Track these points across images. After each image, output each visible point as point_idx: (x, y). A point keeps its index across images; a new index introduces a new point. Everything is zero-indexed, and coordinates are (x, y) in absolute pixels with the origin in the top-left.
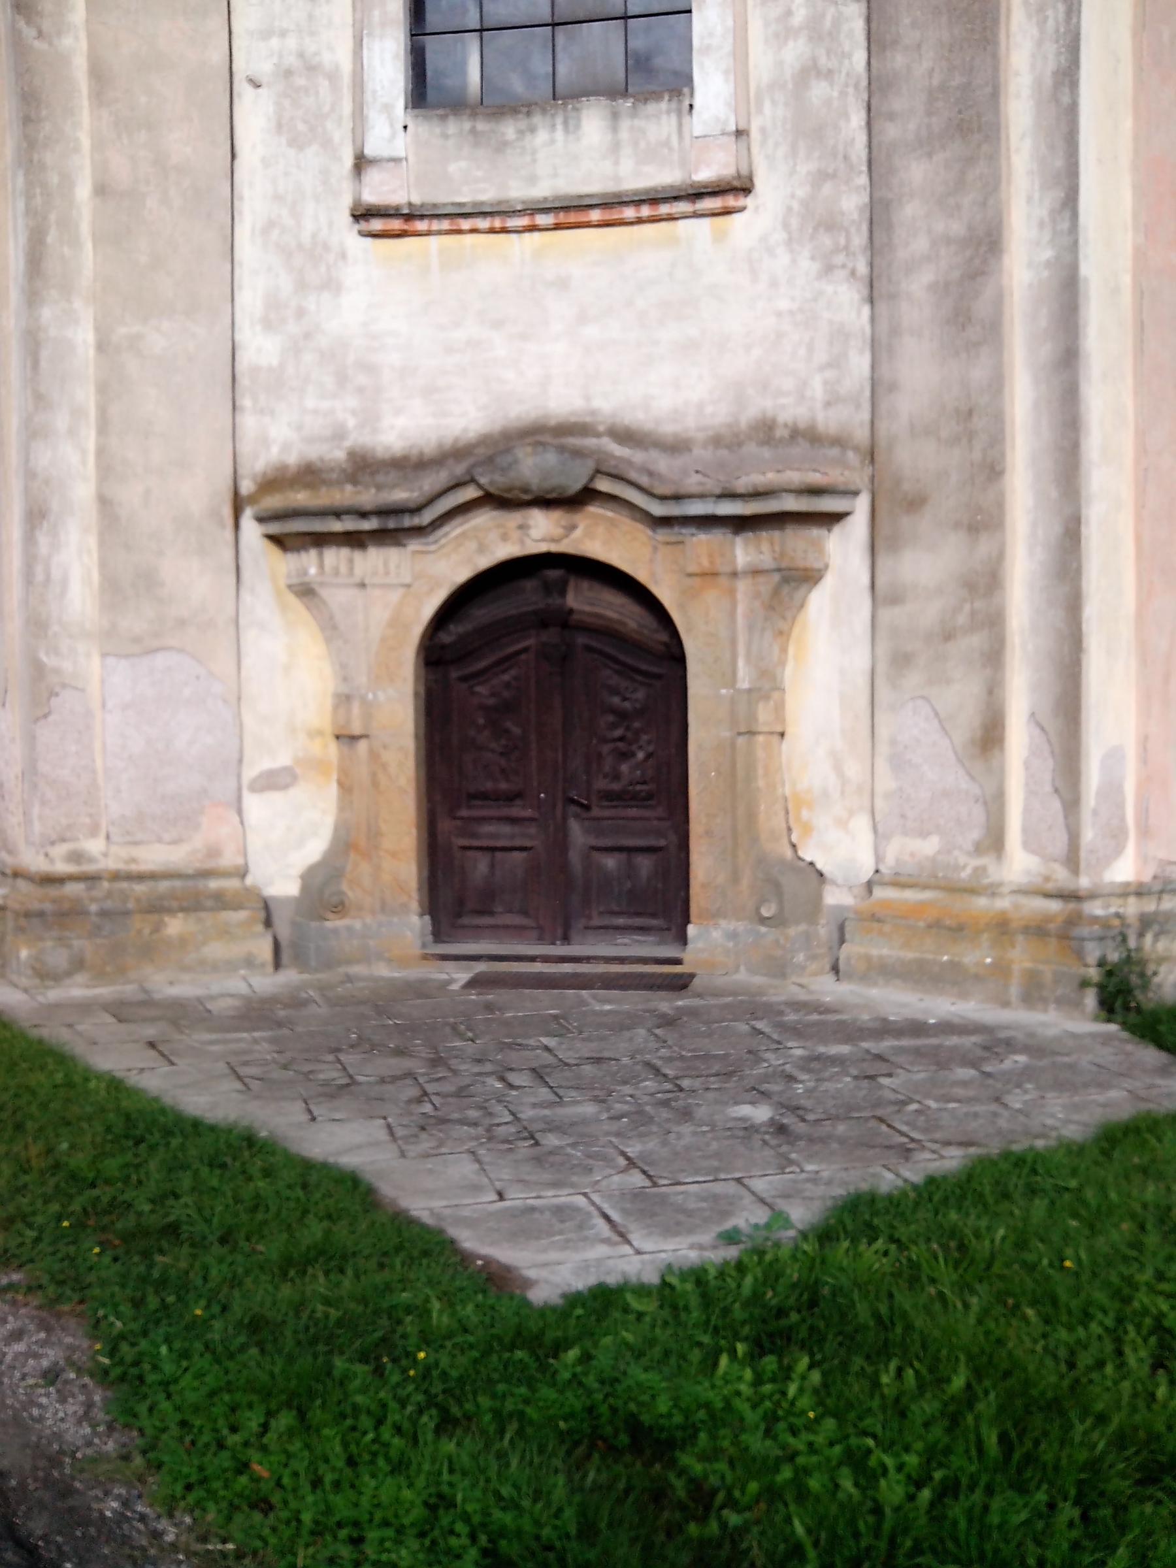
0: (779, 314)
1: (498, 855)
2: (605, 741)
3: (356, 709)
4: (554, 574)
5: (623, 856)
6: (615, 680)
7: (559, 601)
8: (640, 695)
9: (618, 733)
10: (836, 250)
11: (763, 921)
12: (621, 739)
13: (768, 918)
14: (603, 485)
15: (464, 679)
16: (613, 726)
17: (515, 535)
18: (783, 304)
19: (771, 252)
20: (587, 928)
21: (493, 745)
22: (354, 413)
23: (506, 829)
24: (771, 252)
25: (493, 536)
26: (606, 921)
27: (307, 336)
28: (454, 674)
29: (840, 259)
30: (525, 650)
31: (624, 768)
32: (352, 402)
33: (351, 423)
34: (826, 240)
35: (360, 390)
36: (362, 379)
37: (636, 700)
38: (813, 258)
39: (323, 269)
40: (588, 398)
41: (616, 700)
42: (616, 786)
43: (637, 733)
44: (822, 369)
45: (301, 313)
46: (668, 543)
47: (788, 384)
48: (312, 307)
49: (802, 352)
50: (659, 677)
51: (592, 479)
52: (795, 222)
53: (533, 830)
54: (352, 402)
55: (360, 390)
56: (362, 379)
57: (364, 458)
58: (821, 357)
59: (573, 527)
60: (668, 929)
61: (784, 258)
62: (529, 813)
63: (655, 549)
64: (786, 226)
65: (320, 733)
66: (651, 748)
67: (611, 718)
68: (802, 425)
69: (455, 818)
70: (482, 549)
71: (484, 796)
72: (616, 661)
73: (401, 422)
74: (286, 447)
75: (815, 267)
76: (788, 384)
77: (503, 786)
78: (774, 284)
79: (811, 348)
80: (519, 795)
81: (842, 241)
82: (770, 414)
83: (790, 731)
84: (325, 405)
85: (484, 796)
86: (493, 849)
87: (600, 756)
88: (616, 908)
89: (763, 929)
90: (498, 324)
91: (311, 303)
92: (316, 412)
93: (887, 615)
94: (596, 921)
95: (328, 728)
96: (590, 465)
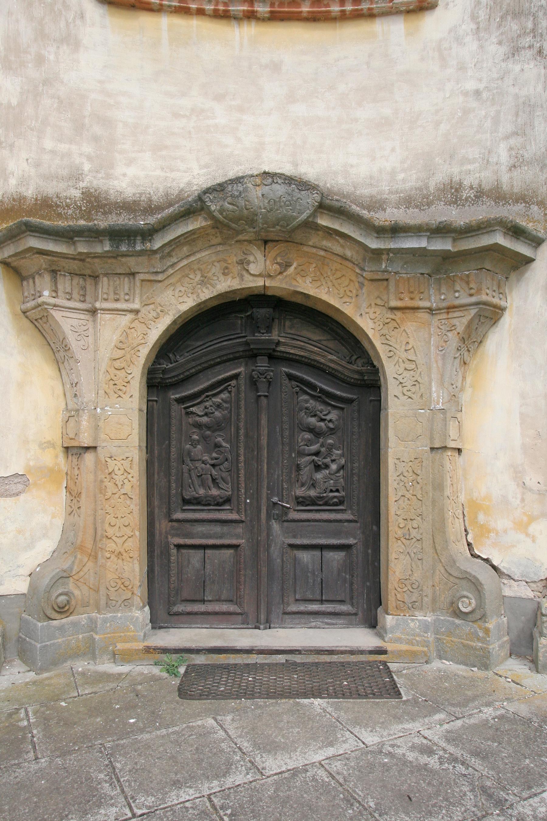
0: (466, 94)
1: (209, 552)
2: (301, 454)
3: (85, 422)
4: (262, 312)
5: (317, 553)
6: (312, 403)
7: (265, 337)
8: (333, 415)
9: (314, 448)
10: (524, 33)
11: (458, 614)
12: (317, 454)
13: (466, 614)
14: (324, 221)
15: (181, 401)
16: (309, 443)
17: (236, 269)
18: (471, 85)
19: (459, 41)
20: (285, 613)
21: (206, 457)
22: (89, 158)
23: (217, 529)
24: (459, 41)
25: (216, 269)
26: (302, 607)
27: (47, 82)
28: (174, 396)
29: (527, 40)
30: (236, 377)
31: (319, 476)
32: (88, 148)
33: (87, 167)
34: (514, 26)
35: (96, 139)
36: (97, 130)
37: (330, 421)
38: (500, 43)
39: (62, 24)
40: (296, 165)
41: (313, 420)
42: (312, 493)
43: (330, 448)
44: (507, 138)
45: (40, 60)
46: (372, 280)
47: (473, 152)
48: (52, 57)
49: (488, 124)
50: (350, 401)
51: (314, 214)
52: (482, 14)
53: (239, 529)
54: (88, 148)
55: (96, 139)
56: (97, 130)
57: (97, 198)
58: (506, 127)
59: (288, 265)
60: (356, 614)
61: (472, 45)
62: (234, 516)
63: (362, 285)
64: (474, 17)
65: (51, 444)
66: (343, 461)
67: (308, 436)
68: (486, 187)
69: (172, 521)
70: (205, 282)
71: (197, 501)
72: (313, 387)
73: (132, 171)
74: (24, 181)
75: (502, 50)
76: (473, 152)
77: (214, 492)
78: (462, 68)
79: (496, 121)
80: (228, 501)
81: (530, 25)
82: (456, 179)
83: (466, 447)
84: (63, 147)
85: (197, 501)
86: (204, 547)
87: (298, 468)
88: (311, 597)
89: (457, 621)
90: (219, 98)
91: (50, 53)
92: (53, 152)
93: (379, 398)
94: (293, 608)
95: (59, 443)
96: (312, 199)
